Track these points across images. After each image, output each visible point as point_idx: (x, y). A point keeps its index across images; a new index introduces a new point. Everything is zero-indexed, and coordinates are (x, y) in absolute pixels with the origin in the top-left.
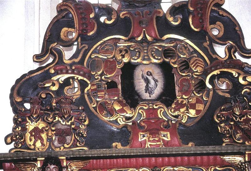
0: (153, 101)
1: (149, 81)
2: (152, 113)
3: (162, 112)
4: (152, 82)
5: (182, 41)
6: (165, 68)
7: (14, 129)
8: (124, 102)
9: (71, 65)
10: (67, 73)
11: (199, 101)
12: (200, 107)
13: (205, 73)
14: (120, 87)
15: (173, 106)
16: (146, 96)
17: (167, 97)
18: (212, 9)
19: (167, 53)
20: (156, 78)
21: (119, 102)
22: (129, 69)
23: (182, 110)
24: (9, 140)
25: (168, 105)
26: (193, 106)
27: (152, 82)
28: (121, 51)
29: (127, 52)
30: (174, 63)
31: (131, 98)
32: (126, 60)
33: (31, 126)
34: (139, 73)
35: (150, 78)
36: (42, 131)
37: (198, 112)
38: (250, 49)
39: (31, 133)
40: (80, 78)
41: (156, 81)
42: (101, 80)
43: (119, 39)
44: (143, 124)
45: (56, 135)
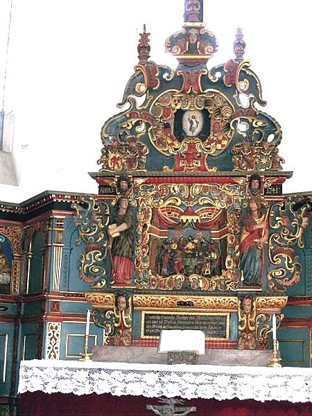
0: (193, 138)
1: (193, 123)
2: (192, 146)
3: (200, 147)
4: (195, 123)
5: (219, 94)
6: (205, 113)
7: (102, 157)
8: (175, 138)
9: (140, 111)
10: (138, 117)
11: (224, 138)
12: (225, 143)
13: (231, 118)
14: (172, 127)
15: (207, 141)
16: (190, 134)
17: (204, 135)
18: (141, 311)
19: (207, 103)
20: (198, 120)
21: (171, 138)
22: (180, 113)
23: (212, 145)
24: (99, 162)
25: (203, 141)
26: (220, 142)
27: (195, 123)
28: (175, 101)
29: (179, 101)
30: (211, 110)
31: (180, 135)
32: (178, 107)
33: (111, 155)
34: (186, 117)
35: (194, 120)
36: (118, 159)
37: (223, 146)
38: (3, 183)
39: (111, 160)
40: (146, 121)
41: (197, 123)
42: (160, 122)
43: (175, 92)
44: (183, 155)
45: (126, 162)
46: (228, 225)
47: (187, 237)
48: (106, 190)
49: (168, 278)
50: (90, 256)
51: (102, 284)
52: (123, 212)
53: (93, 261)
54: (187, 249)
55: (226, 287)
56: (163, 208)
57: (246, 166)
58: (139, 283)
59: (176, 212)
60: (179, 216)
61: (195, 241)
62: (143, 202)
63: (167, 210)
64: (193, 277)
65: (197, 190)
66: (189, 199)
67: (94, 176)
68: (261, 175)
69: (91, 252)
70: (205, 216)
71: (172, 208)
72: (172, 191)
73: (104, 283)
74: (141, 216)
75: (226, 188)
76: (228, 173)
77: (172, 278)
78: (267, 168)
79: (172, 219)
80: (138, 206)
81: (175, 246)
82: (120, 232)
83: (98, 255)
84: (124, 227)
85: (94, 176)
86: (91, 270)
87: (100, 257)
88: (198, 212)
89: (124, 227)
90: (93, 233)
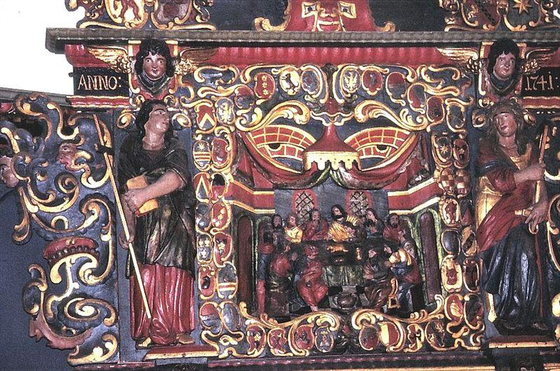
46: (436, 174)
47: (327, 209)
48: (98, 82)
49: (295, 323)
50: (62, 271)
51: (106, 351)
52: (153, 139)
53: (73, 286)
54: (331, 242)
55: (450, 341)
56: (261, 131)
57: (477, 17)
58: (216, 340)
59: (293, 141)
60: (302, 154)
61: (350, 219)
62: (207, 116)
63: (269, 138)
64: (361, 319)
65: (352, 83)
66: (332, 106)
67: (57, 42)
68: (520, 40)
69: (66, 260)
70: (368, 151)
71: (284, 131)
72: (285, 85)
73: (112, 346)
74: (200, 157)
75: (425, 77)
76: (424, 36)
77: (305, 322)
78: (531, 24)
79: (280, 160)
80: (195, 127)
81: (294, 234)
82: (158, 199)
83: (87, 265)
84: (169, 182)
85: (57, 42)
86: (72, 313)
87: (96, 273)
88: (353, 141)
89: (169, 182)
90: (66, 205)
